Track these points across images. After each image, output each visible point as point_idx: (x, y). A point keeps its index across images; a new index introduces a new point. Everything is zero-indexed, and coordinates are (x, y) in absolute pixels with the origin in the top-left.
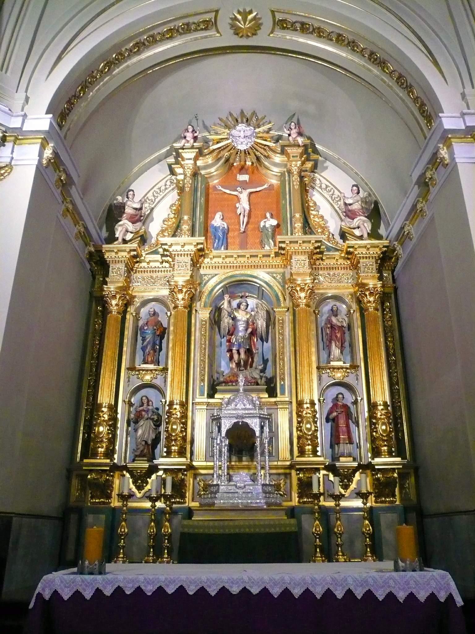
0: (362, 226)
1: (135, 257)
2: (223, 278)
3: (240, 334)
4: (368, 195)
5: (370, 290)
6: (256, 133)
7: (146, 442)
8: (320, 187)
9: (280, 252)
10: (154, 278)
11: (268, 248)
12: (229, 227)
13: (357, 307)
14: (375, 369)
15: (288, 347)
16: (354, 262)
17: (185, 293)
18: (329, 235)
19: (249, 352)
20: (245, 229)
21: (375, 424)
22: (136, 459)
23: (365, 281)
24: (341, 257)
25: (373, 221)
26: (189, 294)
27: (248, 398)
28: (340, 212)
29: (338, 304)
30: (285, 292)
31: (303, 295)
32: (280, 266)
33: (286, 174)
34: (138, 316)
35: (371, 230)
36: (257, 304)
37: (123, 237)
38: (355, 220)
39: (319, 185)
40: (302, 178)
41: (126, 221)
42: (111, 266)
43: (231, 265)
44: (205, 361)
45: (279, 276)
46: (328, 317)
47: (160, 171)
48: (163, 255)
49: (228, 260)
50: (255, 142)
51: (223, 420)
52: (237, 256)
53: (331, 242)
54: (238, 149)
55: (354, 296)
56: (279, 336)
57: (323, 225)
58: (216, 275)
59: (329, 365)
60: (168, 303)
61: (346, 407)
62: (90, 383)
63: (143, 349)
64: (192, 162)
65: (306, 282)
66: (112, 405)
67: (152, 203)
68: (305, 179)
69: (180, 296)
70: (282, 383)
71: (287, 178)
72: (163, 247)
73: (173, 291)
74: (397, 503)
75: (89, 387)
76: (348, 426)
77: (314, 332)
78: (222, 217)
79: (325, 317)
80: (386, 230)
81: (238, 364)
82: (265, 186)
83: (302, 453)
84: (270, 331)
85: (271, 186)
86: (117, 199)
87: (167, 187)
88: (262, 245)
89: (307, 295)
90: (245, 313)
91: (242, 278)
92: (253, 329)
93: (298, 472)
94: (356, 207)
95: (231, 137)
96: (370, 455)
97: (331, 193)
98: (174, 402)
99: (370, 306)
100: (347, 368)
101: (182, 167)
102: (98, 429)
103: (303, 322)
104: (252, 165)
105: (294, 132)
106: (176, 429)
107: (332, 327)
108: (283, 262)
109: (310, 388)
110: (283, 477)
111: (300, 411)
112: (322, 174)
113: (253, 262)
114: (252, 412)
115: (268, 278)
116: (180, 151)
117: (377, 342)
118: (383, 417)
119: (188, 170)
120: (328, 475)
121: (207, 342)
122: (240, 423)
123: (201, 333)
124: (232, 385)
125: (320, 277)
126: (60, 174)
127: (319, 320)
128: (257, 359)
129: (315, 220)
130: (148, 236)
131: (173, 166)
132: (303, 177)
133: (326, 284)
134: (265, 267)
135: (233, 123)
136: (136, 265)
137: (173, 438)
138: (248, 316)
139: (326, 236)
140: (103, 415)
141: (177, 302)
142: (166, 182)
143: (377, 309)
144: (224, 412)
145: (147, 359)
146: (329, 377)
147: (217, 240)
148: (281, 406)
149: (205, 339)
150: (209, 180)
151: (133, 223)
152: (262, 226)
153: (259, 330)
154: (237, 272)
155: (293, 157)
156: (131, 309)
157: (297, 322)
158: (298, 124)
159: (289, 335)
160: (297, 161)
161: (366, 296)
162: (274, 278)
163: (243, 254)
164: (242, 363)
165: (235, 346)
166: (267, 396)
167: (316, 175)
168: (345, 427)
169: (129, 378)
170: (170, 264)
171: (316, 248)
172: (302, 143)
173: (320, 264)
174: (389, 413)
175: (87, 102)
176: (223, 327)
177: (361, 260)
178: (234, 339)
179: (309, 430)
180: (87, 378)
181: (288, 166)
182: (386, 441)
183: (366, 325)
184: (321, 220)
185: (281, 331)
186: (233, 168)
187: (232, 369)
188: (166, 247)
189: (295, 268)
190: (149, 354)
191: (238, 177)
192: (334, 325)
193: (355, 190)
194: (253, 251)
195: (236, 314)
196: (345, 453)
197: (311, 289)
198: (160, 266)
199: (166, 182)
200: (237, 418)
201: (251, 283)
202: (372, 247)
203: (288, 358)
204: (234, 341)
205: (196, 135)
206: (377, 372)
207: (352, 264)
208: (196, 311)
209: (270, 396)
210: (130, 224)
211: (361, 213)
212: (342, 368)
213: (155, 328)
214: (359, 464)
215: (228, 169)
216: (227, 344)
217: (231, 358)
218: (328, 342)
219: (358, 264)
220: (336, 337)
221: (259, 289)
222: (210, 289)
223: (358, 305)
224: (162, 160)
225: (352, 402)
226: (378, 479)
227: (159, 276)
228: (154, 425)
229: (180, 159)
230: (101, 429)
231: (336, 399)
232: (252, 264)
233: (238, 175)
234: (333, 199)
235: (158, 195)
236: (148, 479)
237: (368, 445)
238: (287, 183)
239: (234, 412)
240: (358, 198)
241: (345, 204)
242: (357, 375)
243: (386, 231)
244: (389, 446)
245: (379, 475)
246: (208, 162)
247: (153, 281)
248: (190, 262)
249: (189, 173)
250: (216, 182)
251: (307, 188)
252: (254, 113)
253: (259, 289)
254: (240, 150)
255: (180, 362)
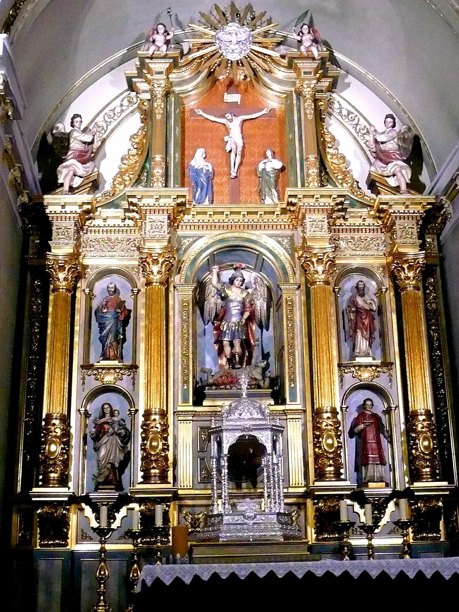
0: (399, 174)
1: (88, 212)
2: (210, 242)
4: (406, 130)
5: (409, 263)
6: (253, 36)
7: (113, 465)
8: (340, 112)
9: (288, 208)
10: (113, 241)
12: (215, 169)
13: (391, 283)
14: (414, 369)
15: (299, 338)
16: (387, 223)
17: (162, 264)
18: (353, 184)
19: (246, 345)
20: (237, 173)
21: (414, 439)
22: (100, 487)
23: (401, 250)
24: (370, 216)
25: (412, 163)
27: (254, 405)
28: (368, 153)
29: (364, 279)
31: (320, 268)
32: (287, 227)
33: (294, 95)
34: (91, 294)
35: (411, 180)
36: (256, 279)
37: (70, 183)
38: (390, 165)
39: (338, 111)
40: (316, 101)
41: (74, 161)
42: (54, 224)
43: (220, 224)
44: (188, 356)
45: (286, 241)
46: (351, 297)
47: (112, 83)
48: (127, 210)
49: (216, 217)
50: (253, 51)
53: (356, 194)
54: (228, 60)
55: (386, 269)
56: (287, 322)
57: (345, 170)
59: (354, 362)
60: (134, 276)
61: (375, 416)
62: (29, 386)
63: (102, 340)
64: (164, 76)
66: (65, 415)
67: (103, 131)
68: (320, 103)
69: (155, 268)
70: (293, 385)
71: (295, 102)
72: (130, 200)
73: (144, 261)
74: (441, 540)
75: (29, 392)
76: (379, 442)
77: (334, 318)
78: (204, 156)
79: (347, 296)
80: (431, 180)
81: (231, 360)
82: (264, 112)
83: (321, 475)
84: (271, 314)
85: (272, 111)
86: (58, 128)
87: (124, 108)
88: (260, 196)
89: (325, 268)
91: (236, 243)
92: (251, 312)
93: (316, 501)
94: (391, 146)
95: (218, 42)
96: (407, 479)
97: (355, 122)
99: (409, 284)
100: (377, 366)
101: (148, 82)
102: (49, 448)
104: (244, 79)
105: (307, 39)
106: (157, 447)
107: (358, 311)
108: (291, 221)
109: (331, 391)
110: (295, 508)
111: (319, 423)
112: (342, 94)
113: (251, 221)
114: (261, 422)
115: (272, 243)
116: (147, 61)
117: (418, 333)
118: (424, 430)
119: (159, 89)
120: (353, 505)
121: (191, 331)
122: (247, 437)
123: (182, 317)
124: (226, 389)
125: (341, 242)
126: (6, 108)
127: (339, 300)
128: (257, 353)
129: (334, 161)
130: (100, 180)
131: (134, 80)
132: (317, 99)
133: (348, 252)
134: (267, 228)
135: (218, 17)
136: (88, 223)
137: (153, 458)
138: (244, 295)
139: (349, 184)
140: (55, 429)
141: (151, 276)
142: (123, 100)
143: (417, 288)
144: (226, 424)
145: (108, 353)
146: (353, 377)
147: (199, 189)
149: (188, 326)
150: (185, 101)
151: (83, 163)
152: (260, 170)
153: (258, 314)
154: (229, 235)
155: (305, 73)
156: (82, 284)
158: (311, 25)
159: (301, 321)
160: (310, 80)
161: (404, 269)
162: (279, 242)
163: (237, 210)
164: (237, 359)
165: (227, 336)
166: (272, 402)
167: (334, 95)
168: (375, 443)
169: (83, 378)
170: (136, 222)
171: (337, 204)
172: (319, 56)
173: (341, 224)
174: (433, 424)
175: (33, 4)
177: (398, 222)
178: (225, 326)
179: (332, 446)
180: (25, 380)
181: (298, 85)
182: (427, 460)
183: (403, 308)
184: (342, 161)
185: (289, 316)
186: (217, 83)
187: (221, 366)
188: (134, 200)
190: (110, 347)
191: (225, 98)
192: (360, 309)
193: (390, 122)
194: (252, 207)
195: (227, 291)
196: (375, 477)
197: (331, 261)
198: (122, 224)
199: (123, 100)
201: (248, 249)
202: (413, 204)
203: (300, 352)
205: (168, 37)
206: (417, 371)
207: (385, 225)
208: (174, 287)
209: (277, 403)
210: (79, 165)
211: (397, 156)
212: (371, 366)
213: (118, 310)
214: (394, 491)
215: (212, 83)
216: (215, 332)
217: (221, 351)
218: (352, 331)
219: (392, 226)
220: (363, 324)
221: (258, 257)
222: (192, 258)
223: (392, 282)
224: (114, 68)
225: (384, 411)
226: (418, 509)
227: (119, 239)
228: (122, 442)
229: (145, 71)
230: (53, 448)
231: (362, 408)
232: (249, 223)
233: (226, 94)
234: (358, 131)
235: (112, 120)
236: (116, 514)
237: (405, 466)
238: (295, 108)
239: (238, 423)
240: (394, 134)
241: (376, 141)
242: (390, 375)
243: (431, 182)
244: (433, 468)
245: (419, 505)
246: (184, 76)
247: (111, 245)
248: (166, 221)
249: (159, 92)
250: (193, 103)
251: (323, 116)
252: (249, 8)
253: (258, 257)
254: (232, 62)
255: (158, 359)
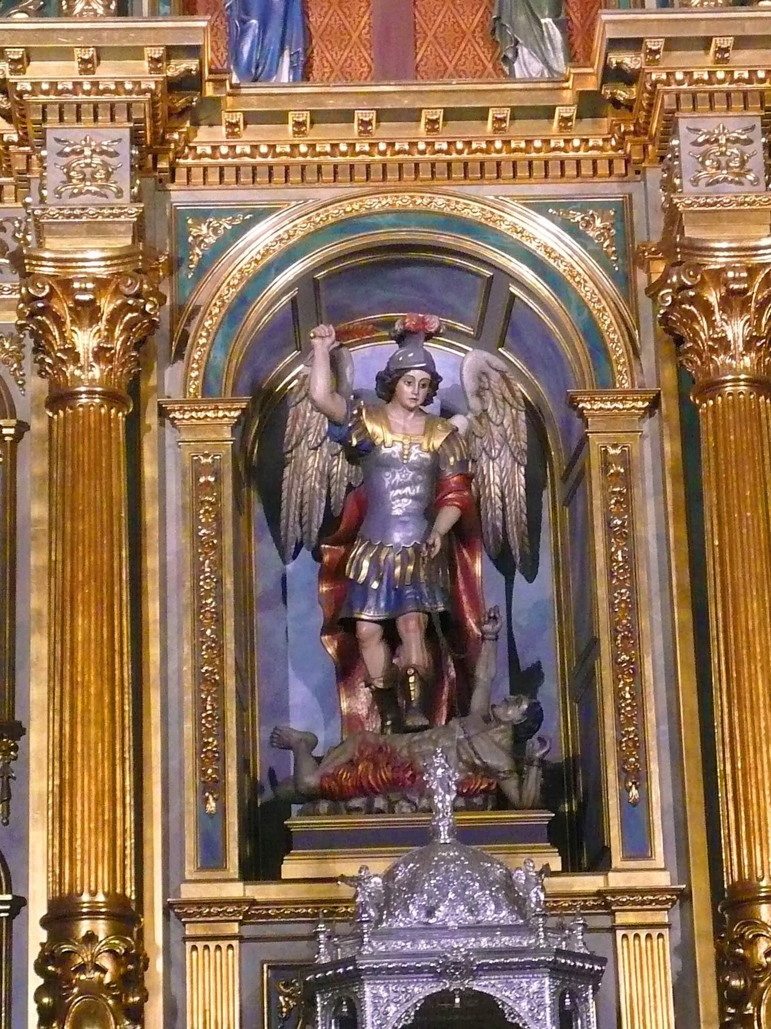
3: (397, 537)
9: (607, 92)
11: (536, 67)
17: (113, 320)
26: (129, 327)
30: (635, 310)
32: (603, 168)
36: (481, 375)
44: (220, 685)
51: (367, 989)
52: (372, 115)
56: (608, 545)
58: (259, 215)
65: (757, 260)
88: (495, 44)
89: (758, 327)
90: (421, 422)
91: (403, 235)
98: (79, 904)
103: (740, 476)
123: (194, 533)
124: (370, 810)
134: (523, 173)
141: (70, 370)
148: (631, 918)
149: (218, 564)
153: (492, 514)
154: (376, 203)
157: (708, 471)
159: (663, 539)
162: (573, 230)
163: (406, 103)
164: (414, 692)
165: (371, 602)
176: (295, 499)
178: (366, 564)
187: (351, 722)
189: (695, 182)
195: (372, 427)
200: (437, 975)
201: (449, 259)
203: (661, 662)
204: (364, 572)
208: (163, 413)
209: (571, 866)
222: (229, 295)
248: (126, 151)
255: (100, 695)
